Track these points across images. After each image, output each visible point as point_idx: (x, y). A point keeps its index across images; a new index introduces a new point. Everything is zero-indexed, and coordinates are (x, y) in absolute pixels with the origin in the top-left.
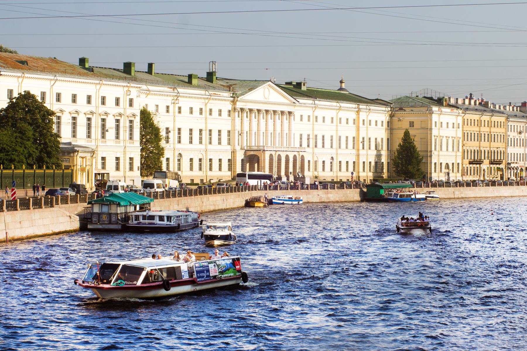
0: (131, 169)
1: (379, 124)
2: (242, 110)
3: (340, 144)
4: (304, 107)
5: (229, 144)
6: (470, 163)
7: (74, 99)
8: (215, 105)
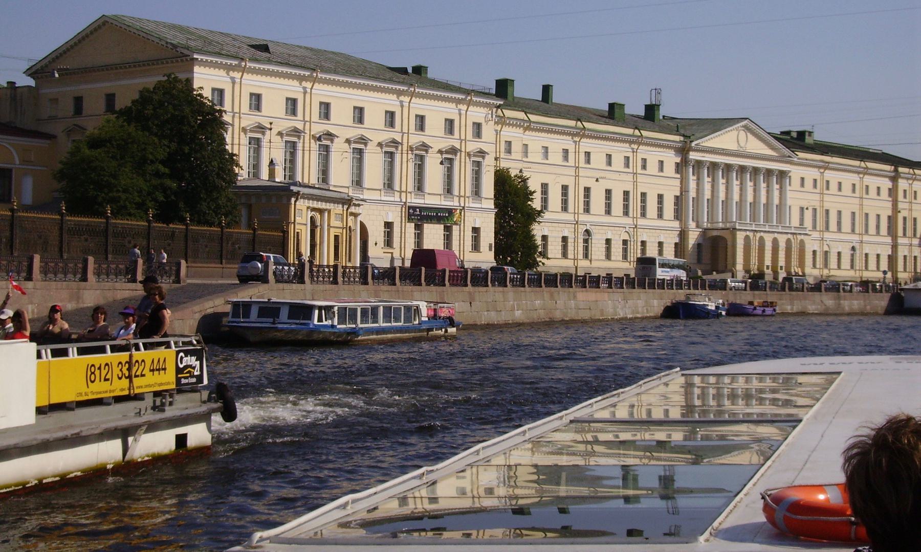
0: (476, 247)
3: (867, 225)
4: (802, 170)
7: (359, 114)
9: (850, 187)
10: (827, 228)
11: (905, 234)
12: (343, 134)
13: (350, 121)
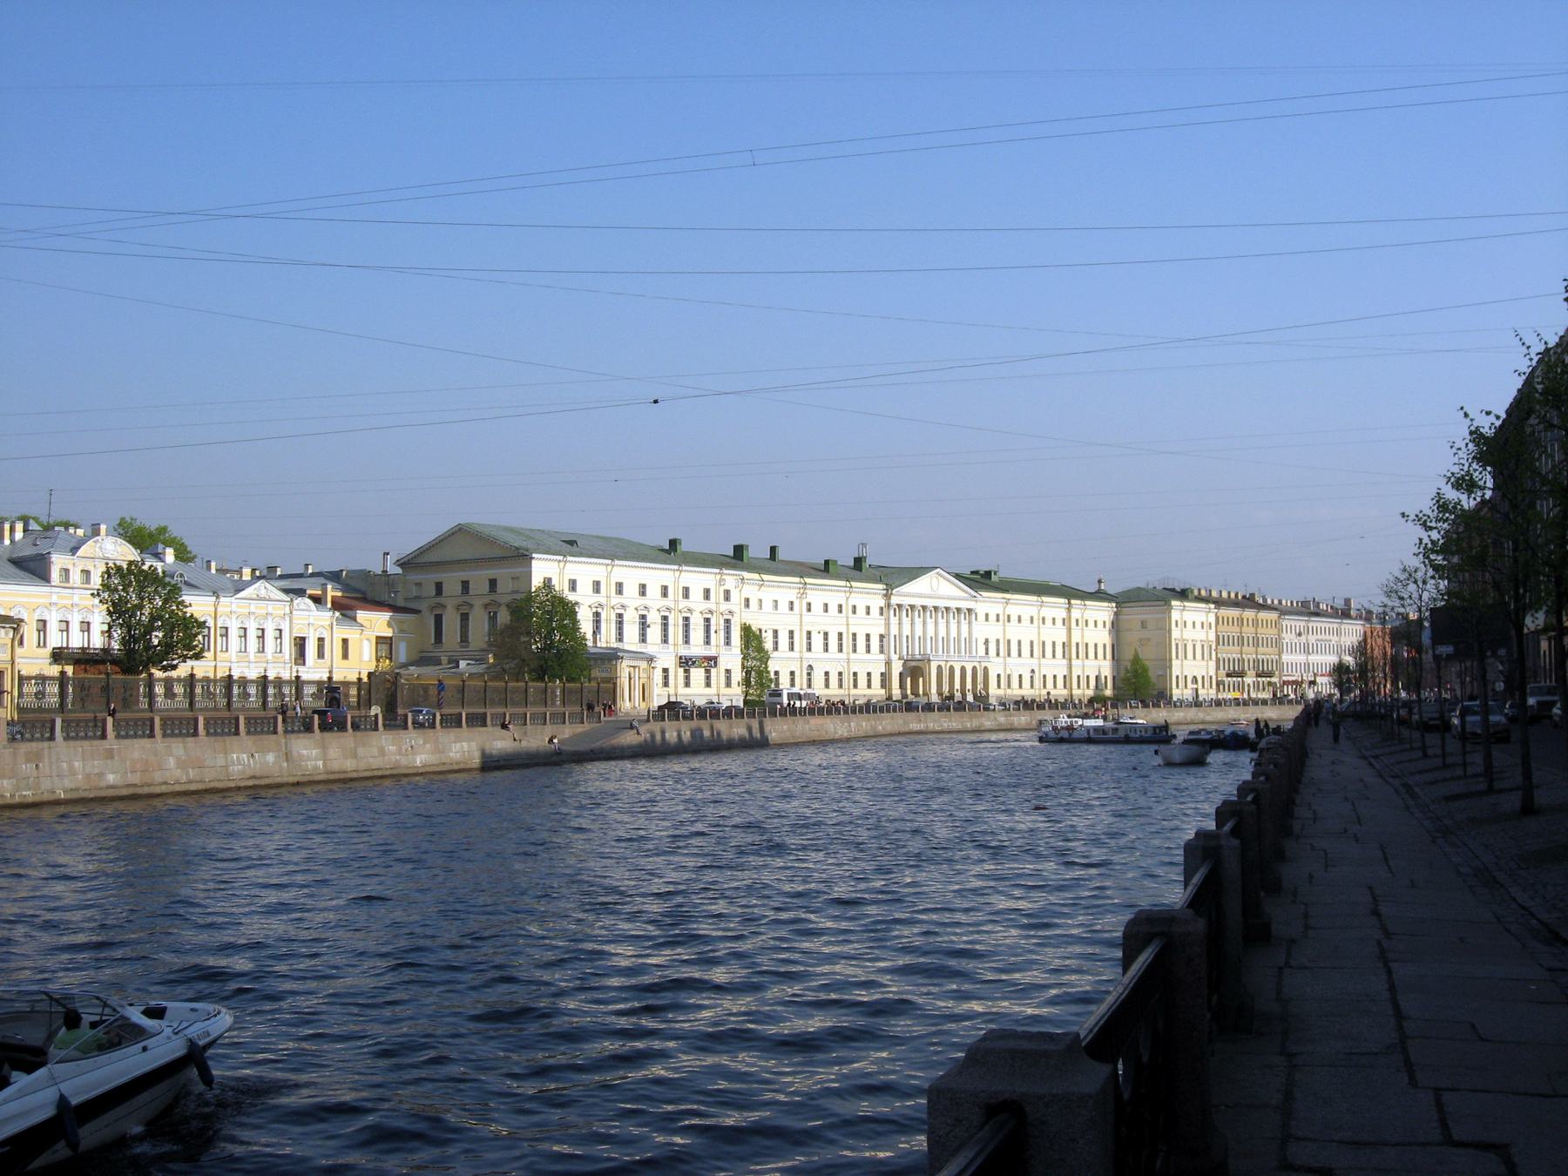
0: (728, 684)
1: (1100, 624)
2: (900, 606)
4: (989, 603)
5: (882, 652)
6: (1228, 675)
7: (643, 590)
8: (861, 601)
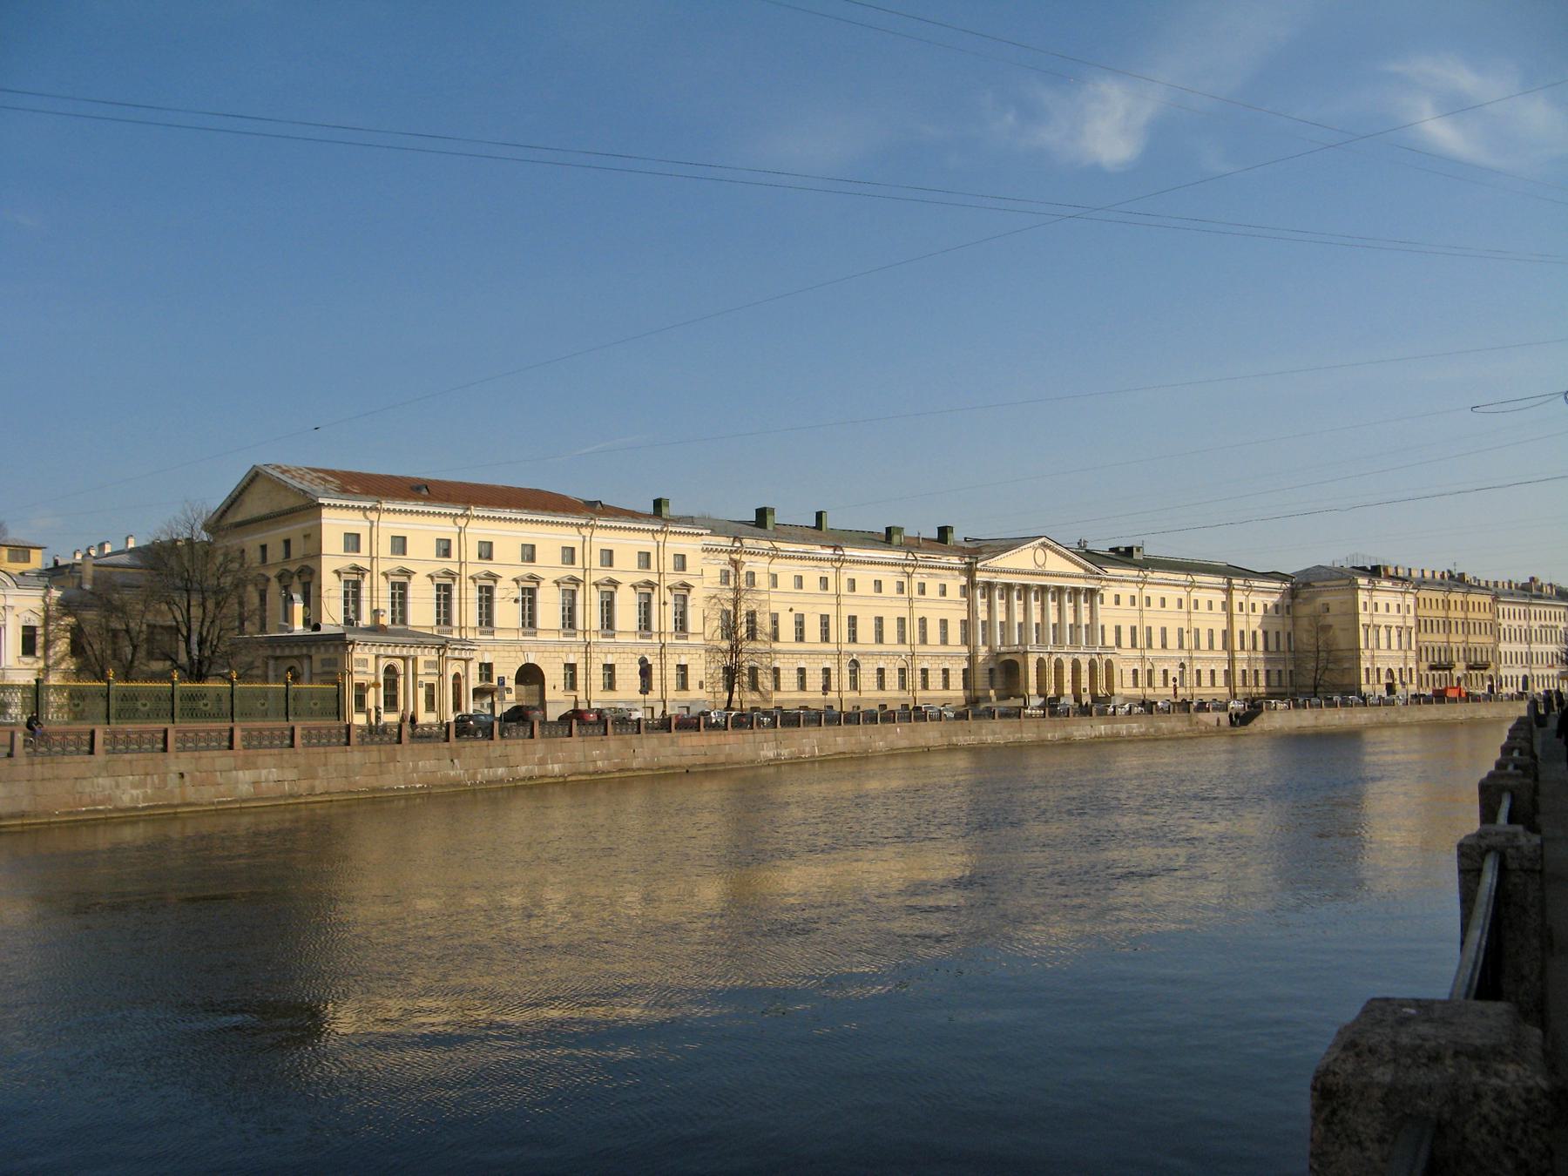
4: (1120, 586)
6: (1432, 668)
7: (529, 553)
9: (1176, 603)
10: (1150, 646)
11: (1242, 648)
12: (626, 580)
13: (558, 562)
